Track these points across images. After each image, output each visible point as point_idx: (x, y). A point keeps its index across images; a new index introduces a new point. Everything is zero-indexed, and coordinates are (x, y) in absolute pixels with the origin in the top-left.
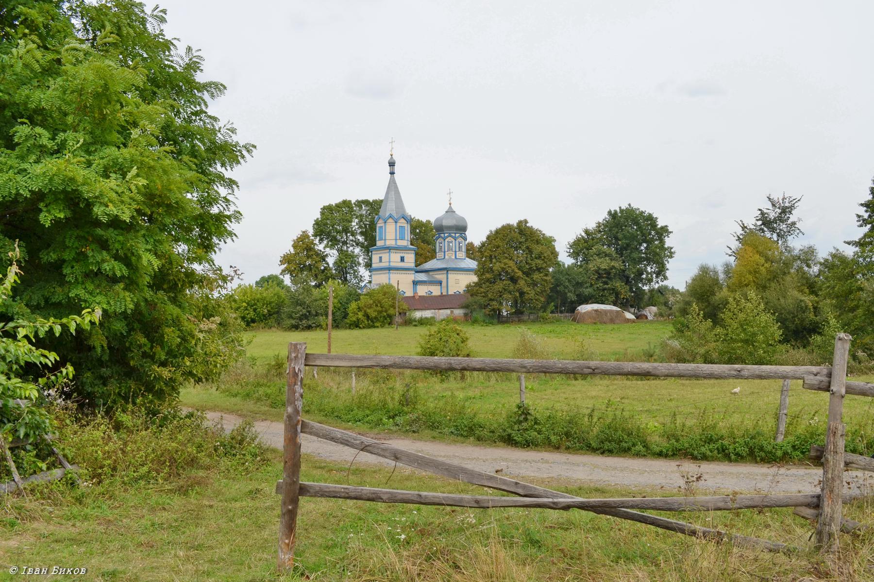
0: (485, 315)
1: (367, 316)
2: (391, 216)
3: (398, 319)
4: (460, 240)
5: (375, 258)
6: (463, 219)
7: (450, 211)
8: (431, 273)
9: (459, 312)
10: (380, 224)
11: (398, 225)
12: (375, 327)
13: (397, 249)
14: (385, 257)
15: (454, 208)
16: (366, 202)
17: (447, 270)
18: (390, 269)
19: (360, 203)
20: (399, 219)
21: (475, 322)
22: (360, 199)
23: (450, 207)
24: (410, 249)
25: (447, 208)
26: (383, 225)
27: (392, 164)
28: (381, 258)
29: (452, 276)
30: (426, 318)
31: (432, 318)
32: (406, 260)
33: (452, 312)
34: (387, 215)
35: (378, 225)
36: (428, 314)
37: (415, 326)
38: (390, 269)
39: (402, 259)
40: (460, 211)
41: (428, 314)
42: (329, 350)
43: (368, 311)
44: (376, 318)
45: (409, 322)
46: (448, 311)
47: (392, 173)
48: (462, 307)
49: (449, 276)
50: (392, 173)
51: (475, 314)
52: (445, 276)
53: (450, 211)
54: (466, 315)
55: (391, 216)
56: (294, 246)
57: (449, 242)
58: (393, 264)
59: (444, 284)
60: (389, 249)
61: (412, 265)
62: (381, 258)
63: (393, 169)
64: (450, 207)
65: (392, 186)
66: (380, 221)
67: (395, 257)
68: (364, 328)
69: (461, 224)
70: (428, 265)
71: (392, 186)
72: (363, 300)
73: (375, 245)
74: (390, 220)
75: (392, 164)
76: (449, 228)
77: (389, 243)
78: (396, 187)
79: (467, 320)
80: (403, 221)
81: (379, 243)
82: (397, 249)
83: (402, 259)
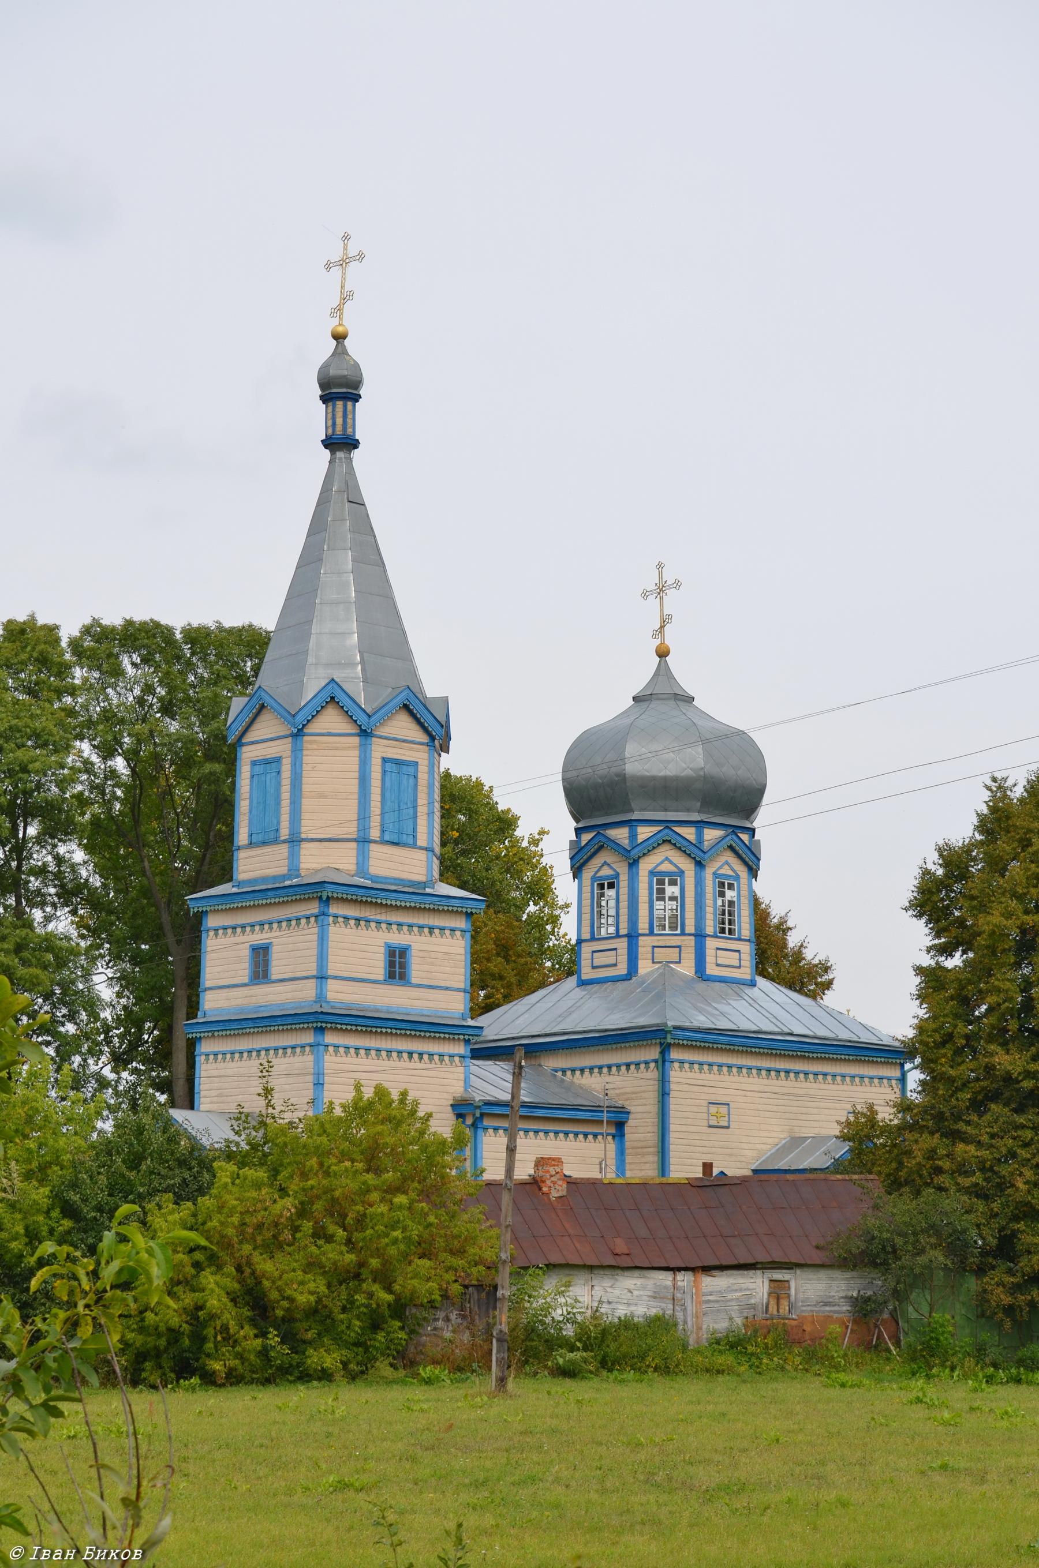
0: (983, 1311)
1: (255, 1301)
2: (333, 699)
3: (447, 1331)
4: (726, 864)
5: (223, 958)
6: (742, 745)
7: (662, 695)
8: (551, 1063)
9: (820, 1293)
10: (263, 743)
11: (379, 750)
12: (305, 1377)
13: (370, 898)
14: (293, 947)
15: (685, 674)
16: (144, 638)
17: (661, 1040)
18: (321, 1022)
19: (104, 644)
20: (383, 713)
21: (927, 1356)
22: (113, 619)
23: (663, 672)
24: (441, 907)
25: (641, 674)
26: (282, 748)
27: (340, 389)
28: (261, 955)
29: (693, 1082)
30: (626, 1324)
31: (660, 1325)
32: (417, 971)
33: (779, 1290)
34: (313, 687)
35: (248, 754)
36: (626, 1297)
37: (568, 1373)
38: (321, 1022)
39: (397, 967)
40: (722, 699)
41: (626, 1297)
42: (778, 1311)
43: (265, 1265)
44: (316, 1312)
45: (536, 1350)
46: (756, 1286)
47: (341, 443)
48: (845, 1263)
49: (676, 1076)
50: (341, 443)
51: (918, 1308)
52: (645, 1081)
53: (662, 695)
54: (863, 1310)
55: (333, 699)
56: (81, 632)
57: (660, 878)
58: (341, 995)
59: (641, 1129)
60: (321, 895)
61: (453, 1005)
62: (261, 955)
63: (348, 418)
64: (663, 672)
65: (340, 518)
66: (266, 727)
67: (357, 950)
68: (233, 1379)
69: (731, 771)
70: (517, 1019)
71: (340, 518)
72: (232, 1193)
73: (226, 874)
74: (331, 721)
75: (340, 389)
76: (666, 791)
77: (327, 861)
78: (364, 528)
79: (874, 1347)
80: (403, 726)
81: (252, 865)
82: (370, 898)
83: (397, 967)
